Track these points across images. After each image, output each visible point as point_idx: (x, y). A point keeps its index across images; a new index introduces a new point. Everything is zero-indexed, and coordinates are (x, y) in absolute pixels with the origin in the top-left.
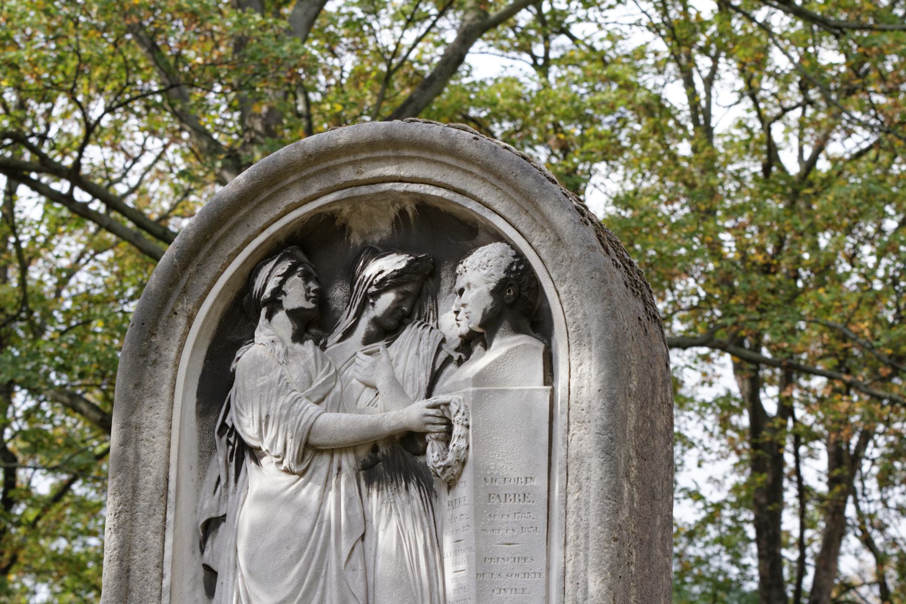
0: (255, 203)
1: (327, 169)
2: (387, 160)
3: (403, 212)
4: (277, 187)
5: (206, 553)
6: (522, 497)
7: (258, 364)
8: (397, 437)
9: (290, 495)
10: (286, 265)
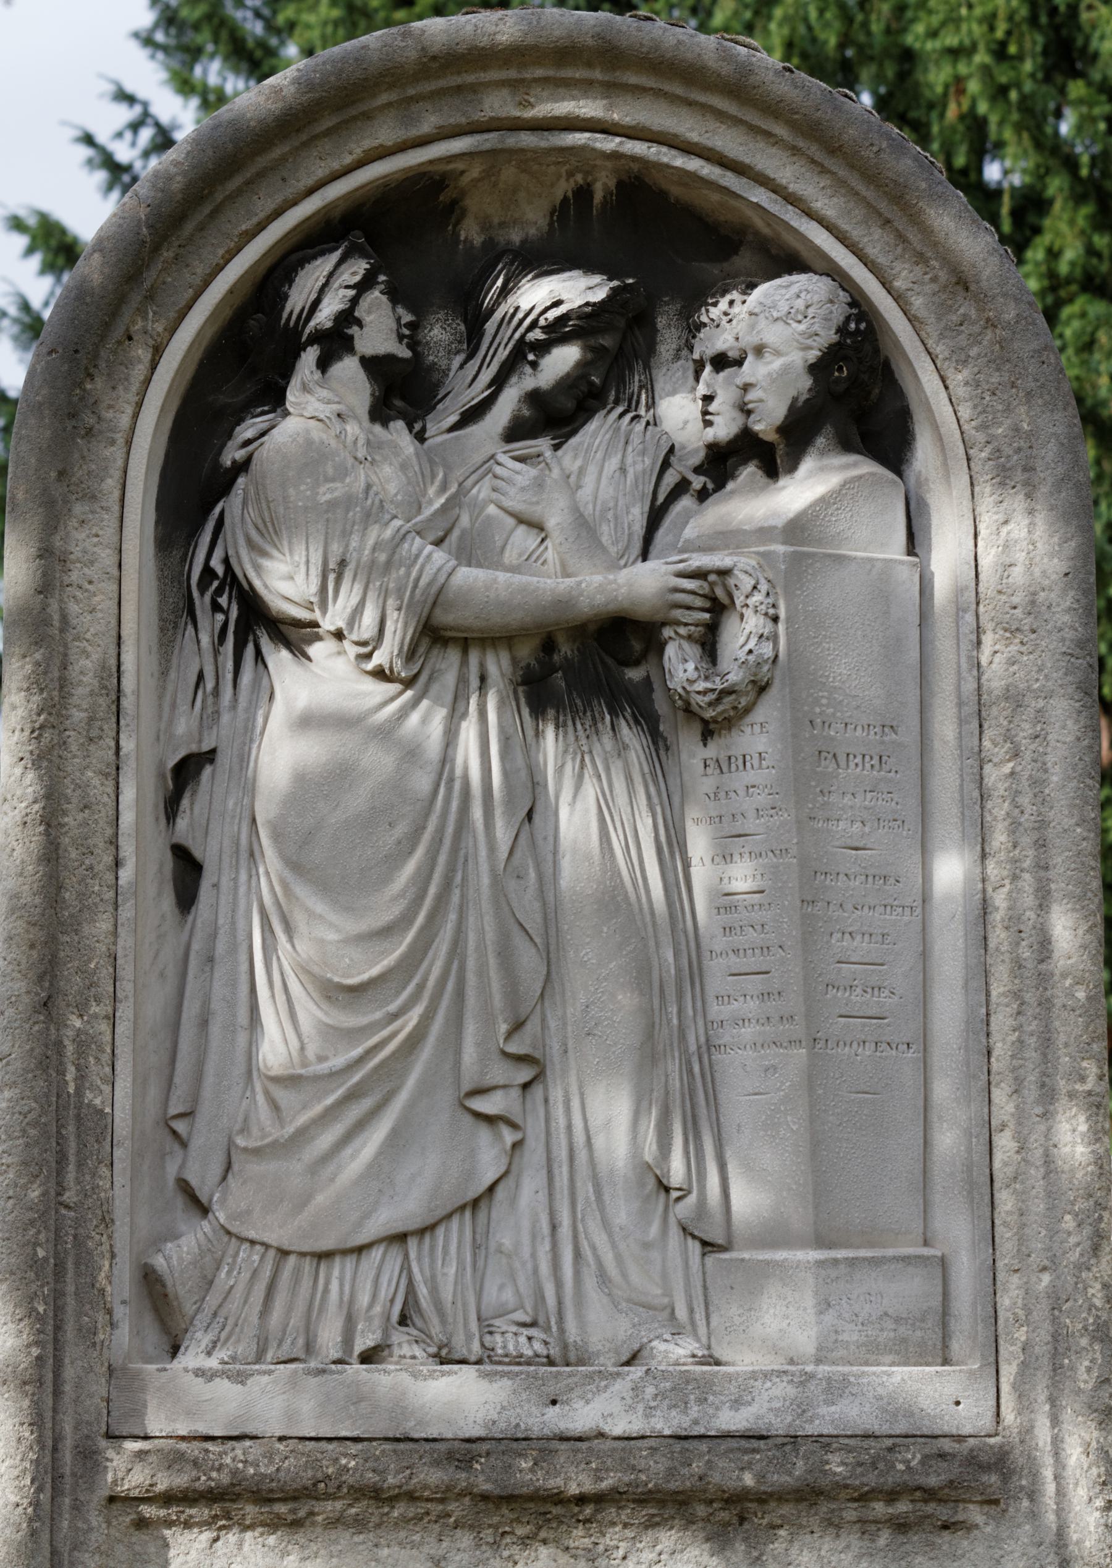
0: (304, 137)
1: (459, 89)
2: (586, 87)
3: (583, 193)
4: (353, 111)
5: (182, 823)
6: (876, 761)
7: (313, 460)
8: (592, 628)
9: (388, 721)
10: (357, 268)
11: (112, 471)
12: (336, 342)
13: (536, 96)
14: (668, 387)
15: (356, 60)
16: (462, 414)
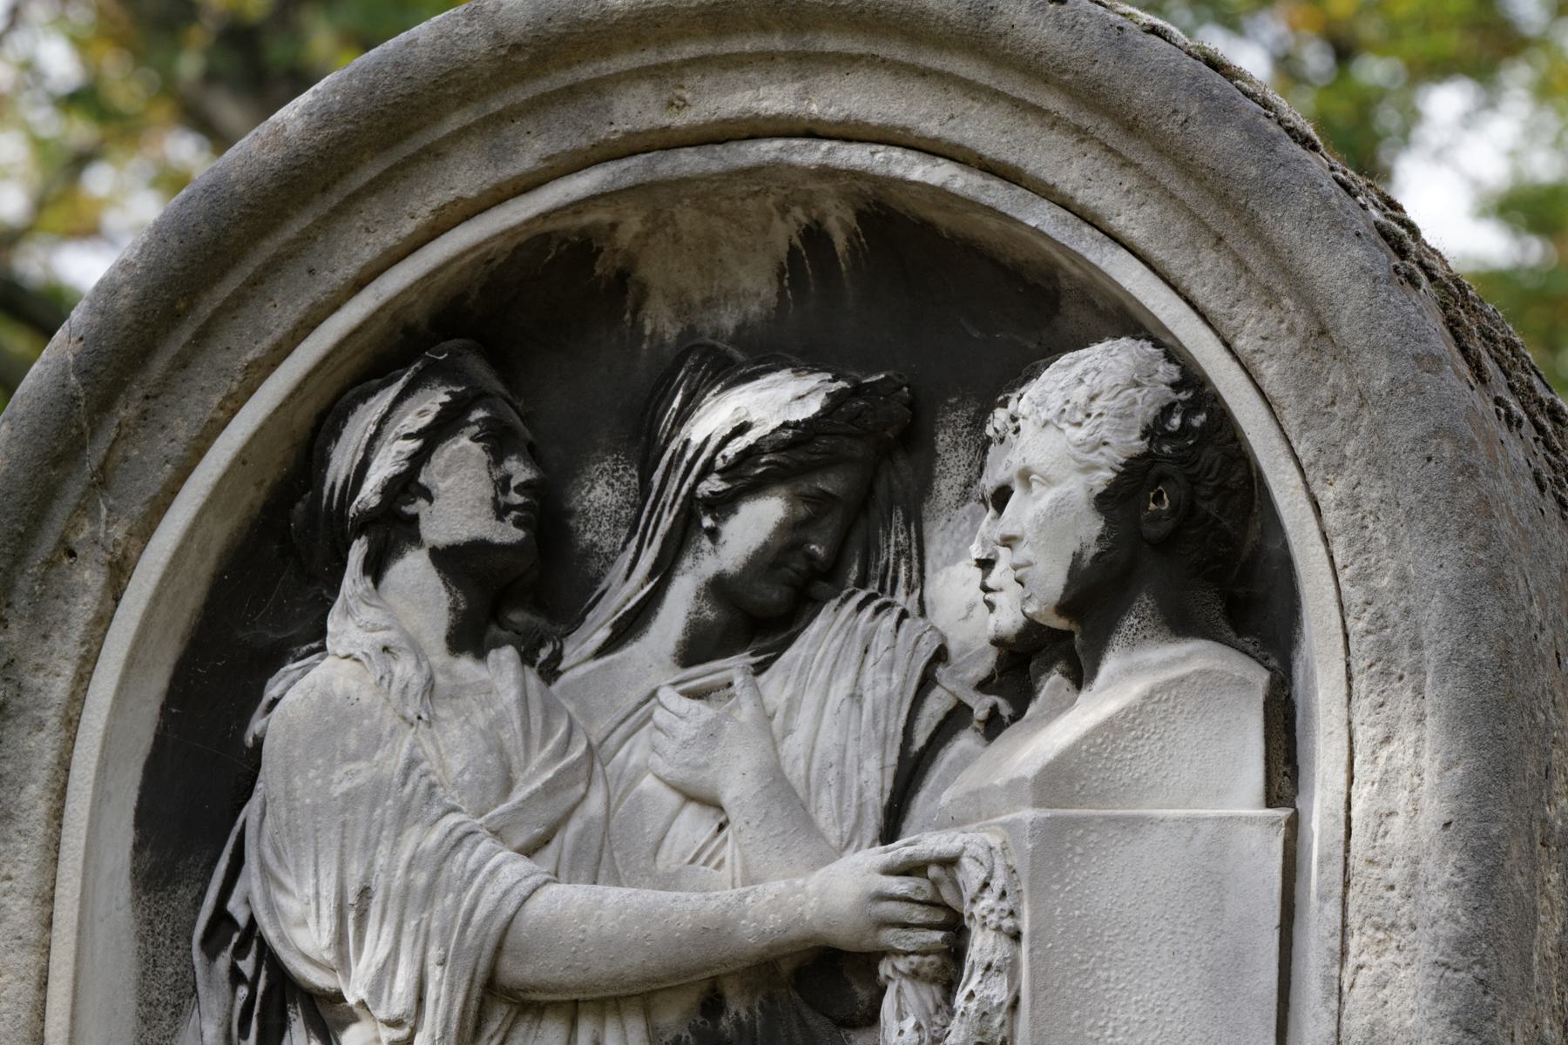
0: (334, 199)
3: (815, 235)
4: (408, 148)
7: (336, 717)
11: (36, 772)
12: (392, 527)
13: (692, 89)
14: (948, 550)
15: (396, 64)
16: (614, 626)
